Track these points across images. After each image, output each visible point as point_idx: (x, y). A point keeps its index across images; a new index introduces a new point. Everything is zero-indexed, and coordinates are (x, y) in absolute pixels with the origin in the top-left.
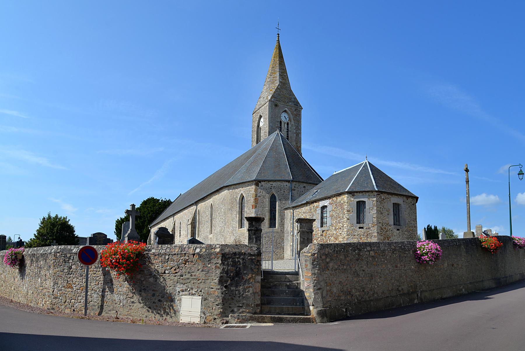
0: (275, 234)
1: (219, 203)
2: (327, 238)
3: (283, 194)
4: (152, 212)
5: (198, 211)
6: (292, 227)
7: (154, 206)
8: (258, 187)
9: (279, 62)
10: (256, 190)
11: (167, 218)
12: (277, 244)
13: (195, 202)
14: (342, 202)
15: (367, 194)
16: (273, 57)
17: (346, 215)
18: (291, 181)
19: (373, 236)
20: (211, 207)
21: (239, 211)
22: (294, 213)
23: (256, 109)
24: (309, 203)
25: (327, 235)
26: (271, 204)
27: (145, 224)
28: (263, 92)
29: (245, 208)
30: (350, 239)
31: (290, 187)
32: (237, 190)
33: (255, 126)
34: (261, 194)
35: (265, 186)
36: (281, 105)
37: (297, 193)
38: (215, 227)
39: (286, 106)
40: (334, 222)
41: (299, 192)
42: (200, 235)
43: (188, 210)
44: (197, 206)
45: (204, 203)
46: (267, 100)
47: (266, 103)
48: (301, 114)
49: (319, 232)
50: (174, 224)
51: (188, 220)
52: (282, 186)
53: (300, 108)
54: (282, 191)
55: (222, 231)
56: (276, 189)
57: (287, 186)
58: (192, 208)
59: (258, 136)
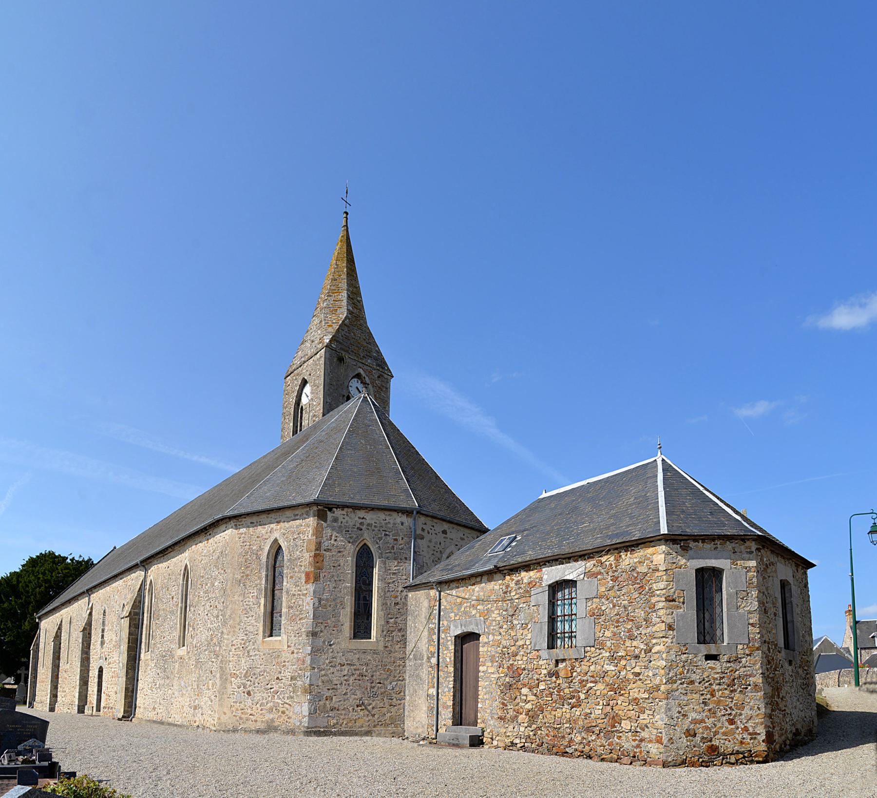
0: (369, 657)
1: (207, 563)
2: (576, 685)
3: (393, 547)
4: (46, 583)
5: (148, 583)
6: (436, 640)
7: (52, 571)
8: (325, 521)
9: (347, 271)
10: (318, 532)
11: (75, 599)
12: (373, 685)
13: (142, 562)
14: (642, 569)
15: (729, 546)
16: (334, 258)
17: (661, 613)
18: (415, 512)
19: (750, 685)
20: (184, 575)
21: (266, 589)
22: (443, 600)
23: (294, 367)
24: (501, 571)
25: (575, 674)
26: (358, 573)
27: (28, 610)
28: (311, 331)
29: (285, 579)
30: (677, 693)
31: (410, 528)
32: (261, 530)
33: (289, 404)
34: (332, 541)
35: (344, 521)
36: (349, 360)
37: (428, 547)
38: (194, 629)
39: (361, 365)
40: (608, 634)
41: (432, 545)
42: (151, 646)
43: (124, 581)
44: (146, 570)
45: (165, 564)
46: (321, 345)
47: (318, 353)
48: (390, 388)
49: (541, 662)
50: (90, 614)
51: (122, 606)
52: (390, 526)
53: (388, 375)
54: (390, 539)
55: (215, 640)
56: (373, 530)
57: (402, 524)
58: (133, 575)
59: (297, 427)
